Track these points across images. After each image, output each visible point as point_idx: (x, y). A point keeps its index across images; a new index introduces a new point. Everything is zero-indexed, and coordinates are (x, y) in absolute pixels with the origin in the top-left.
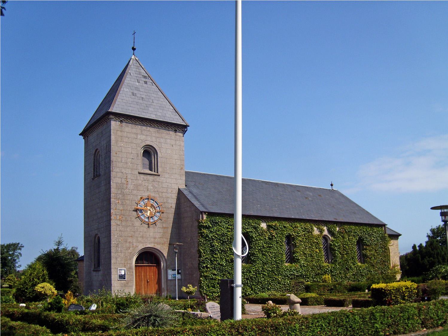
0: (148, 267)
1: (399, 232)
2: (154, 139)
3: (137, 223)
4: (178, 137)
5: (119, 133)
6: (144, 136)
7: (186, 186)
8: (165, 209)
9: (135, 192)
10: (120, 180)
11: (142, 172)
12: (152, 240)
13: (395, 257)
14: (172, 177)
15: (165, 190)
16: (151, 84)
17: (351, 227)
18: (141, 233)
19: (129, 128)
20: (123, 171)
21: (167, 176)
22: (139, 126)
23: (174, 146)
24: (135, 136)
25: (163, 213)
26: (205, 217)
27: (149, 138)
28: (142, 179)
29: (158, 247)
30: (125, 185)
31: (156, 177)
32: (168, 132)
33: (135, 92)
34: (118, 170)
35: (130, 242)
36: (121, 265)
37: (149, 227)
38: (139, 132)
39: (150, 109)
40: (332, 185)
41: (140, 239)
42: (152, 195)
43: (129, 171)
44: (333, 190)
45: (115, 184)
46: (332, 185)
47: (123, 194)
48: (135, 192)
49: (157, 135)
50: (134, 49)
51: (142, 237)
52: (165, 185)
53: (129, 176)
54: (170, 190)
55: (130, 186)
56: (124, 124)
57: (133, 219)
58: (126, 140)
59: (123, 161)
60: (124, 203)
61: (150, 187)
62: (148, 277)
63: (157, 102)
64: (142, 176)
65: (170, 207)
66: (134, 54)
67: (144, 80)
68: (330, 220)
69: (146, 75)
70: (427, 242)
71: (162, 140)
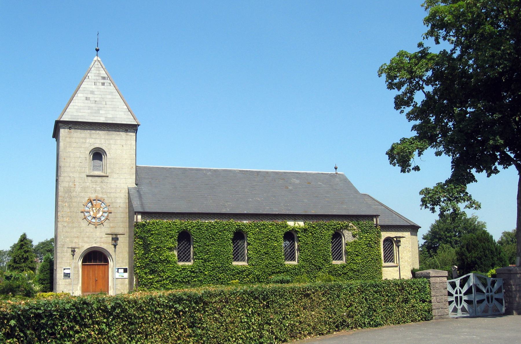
0: (97, 266)
1: (417, 223)
2: (103, 141)
3: (84, 224)
4: (128, 137)
5: (68, 139)
6: (93, 140)
7: (136, 184)
8: (112, 209)
9: (82, 194)
10: (68, 183)
11: (92, 174)
12: (99, 240)
13: (405, 252)
14: (122, 177)
15: (113, 191)
16: (109, 84)
17: (276, 221)
18: (88, 234)
19: (78, 134)
20: (71, 175)
21: (116, 176)
22: (88, 131)
23: (124, 146)
24: (84, 141)
25: (111, 213)
26: (139, 217)
27: (98, 141)
28: (89, 181)
29: (104, 246)
30: (72, 189)
31: (104, 178)
32: (118, 133)
33: (89, 96)
34: (66, 174)
35: (76, 242)
36: (66, 264)
37: (96, 227)
38: (88, 135)
39: (101, 112)
40: (336, 168)
41: (86, 239)
42: (100, 196)
43: (76, 175)
44: (337, 173)
45: (62, 188)
46: (336, 168)
47: (71, 198)
48: (82, 194)
49: (107, 137)
50: (97, 50)
51: (88, 237)
52: (113, 186)
53: (77, 180)
54: (118, 191)
55: (78, 189)
56: (72, 130)
57: (80, 220)
58: (74, 145)
59: (72, 166)
60: (71, 206)
61: (98, 188)
62: (96, 275)
63: (110, 103)
64: (90, 178)
65: (118, 206)
66: (97, 55)
67: (103, 81)
68: (277, 213)
69: (106, 76)
70: (506, 234)
71: (112, 142)
